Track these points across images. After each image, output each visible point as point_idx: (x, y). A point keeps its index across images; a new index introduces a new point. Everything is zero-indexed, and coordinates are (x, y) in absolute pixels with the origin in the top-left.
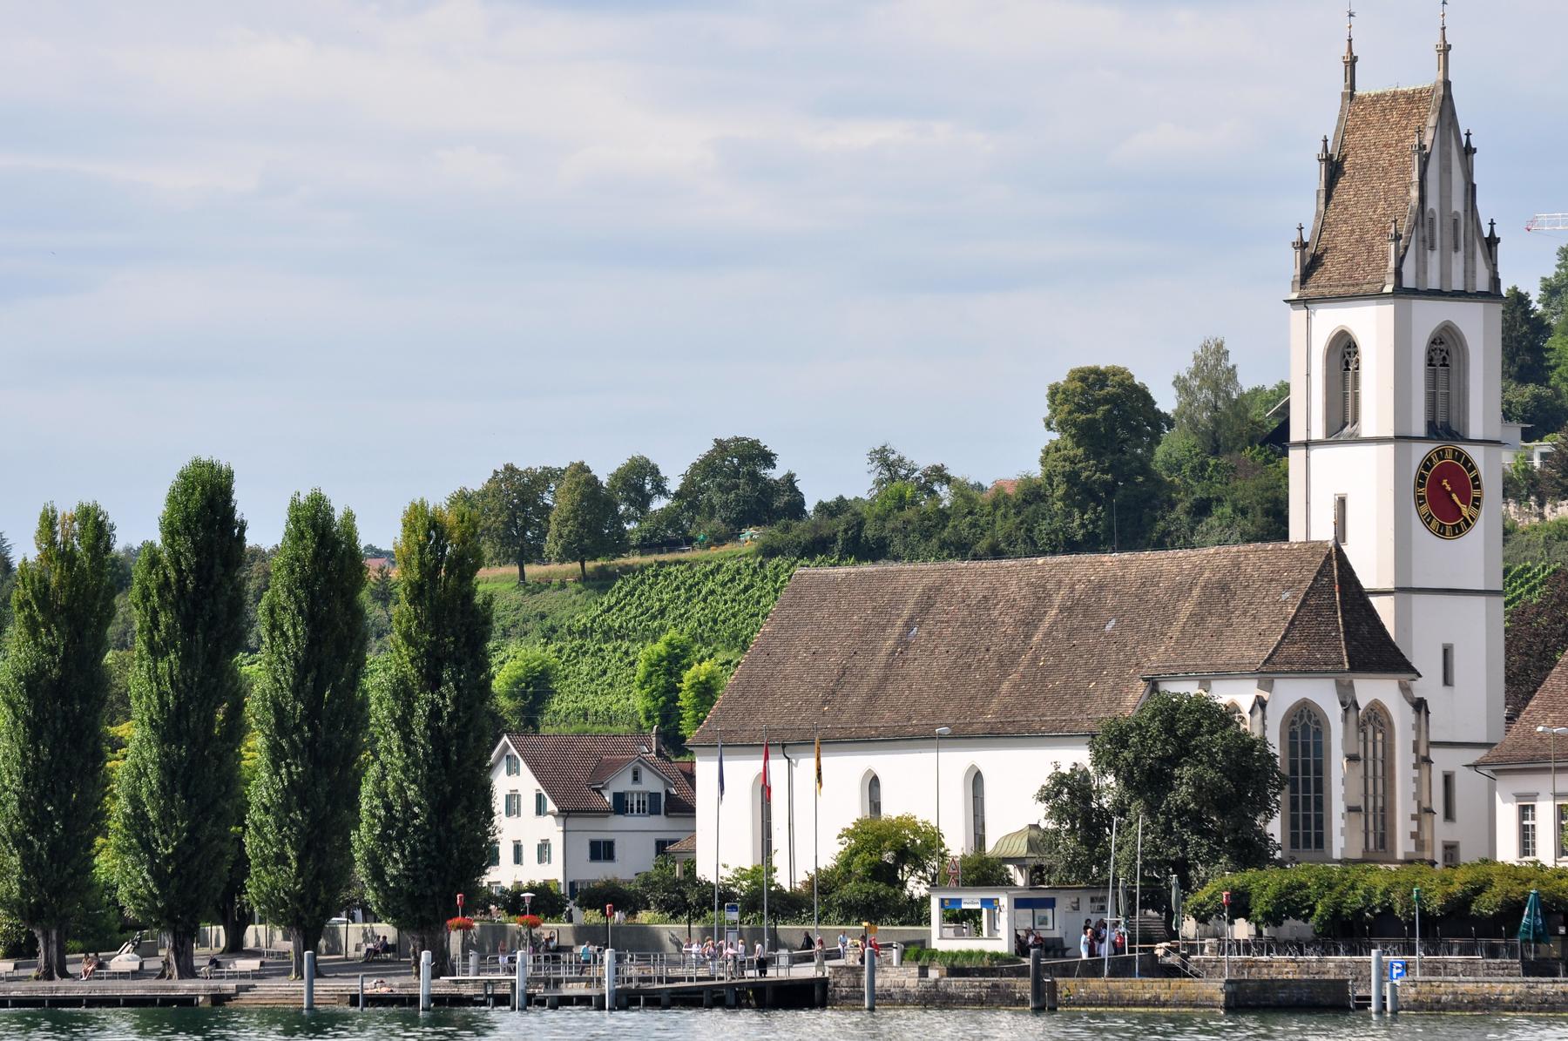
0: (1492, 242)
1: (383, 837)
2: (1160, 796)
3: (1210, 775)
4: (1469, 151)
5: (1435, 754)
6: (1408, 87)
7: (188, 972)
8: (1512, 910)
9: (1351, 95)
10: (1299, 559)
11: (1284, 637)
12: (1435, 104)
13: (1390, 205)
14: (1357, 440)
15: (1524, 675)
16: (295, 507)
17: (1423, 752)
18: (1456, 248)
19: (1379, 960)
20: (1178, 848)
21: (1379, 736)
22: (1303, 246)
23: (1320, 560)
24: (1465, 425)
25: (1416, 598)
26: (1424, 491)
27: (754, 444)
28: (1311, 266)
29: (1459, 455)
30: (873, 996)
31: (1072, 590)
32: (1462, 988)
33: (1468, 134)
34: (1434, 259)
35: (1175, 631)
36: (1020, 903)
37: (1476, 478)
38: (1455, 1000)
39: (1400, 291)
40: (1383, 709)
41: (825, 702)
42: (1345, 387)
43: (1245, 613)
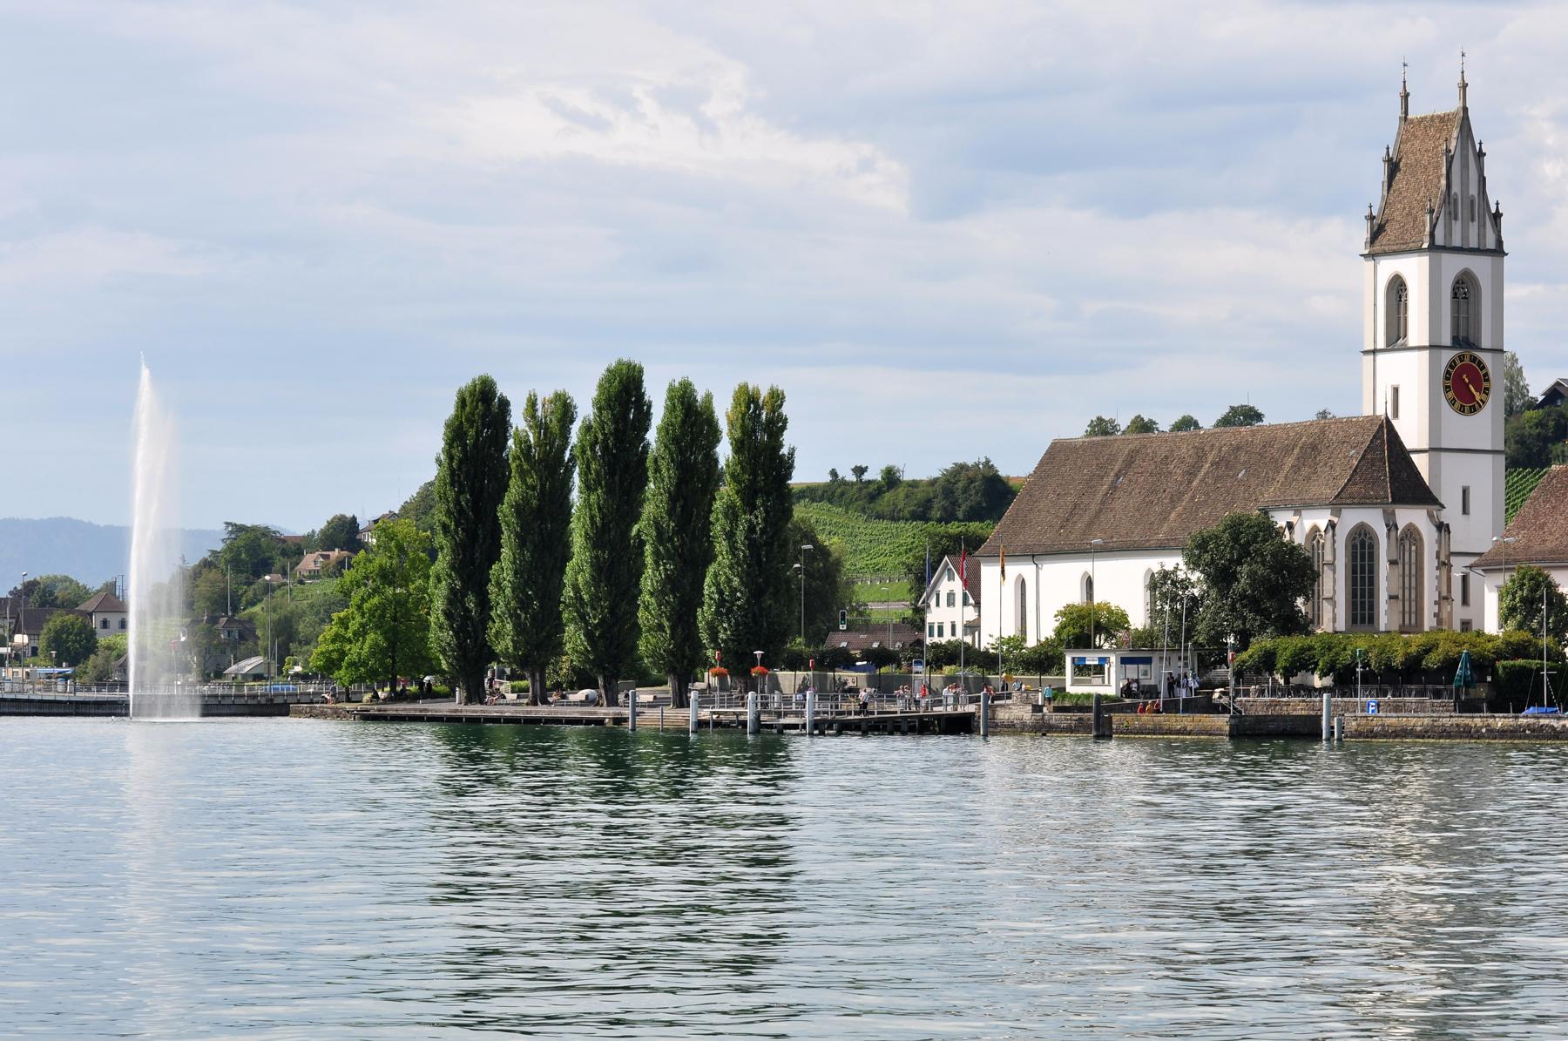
0: (1497, 216)
1: (717, 612)
2: (1229, 587)
4: (1481, 155)
5: (1453, 560)
6: (1441, 112)
7: (682, 702)
8: (1450, 665)
12: (1457, 123)
14: (1406, 348)
16: (671, 389)
19: (1329, 702)
22: (1371, 218)
24: (1479, 338)
25: (1443, 454)
26: (1449, 383)
27: (1252, 409)
28: (1377, 232)
29: (1474, 359)
30: (986, 727)
32: (1388, 721)
34: (1457, 227)
35: (1281, 477)
39: (1433, 247)
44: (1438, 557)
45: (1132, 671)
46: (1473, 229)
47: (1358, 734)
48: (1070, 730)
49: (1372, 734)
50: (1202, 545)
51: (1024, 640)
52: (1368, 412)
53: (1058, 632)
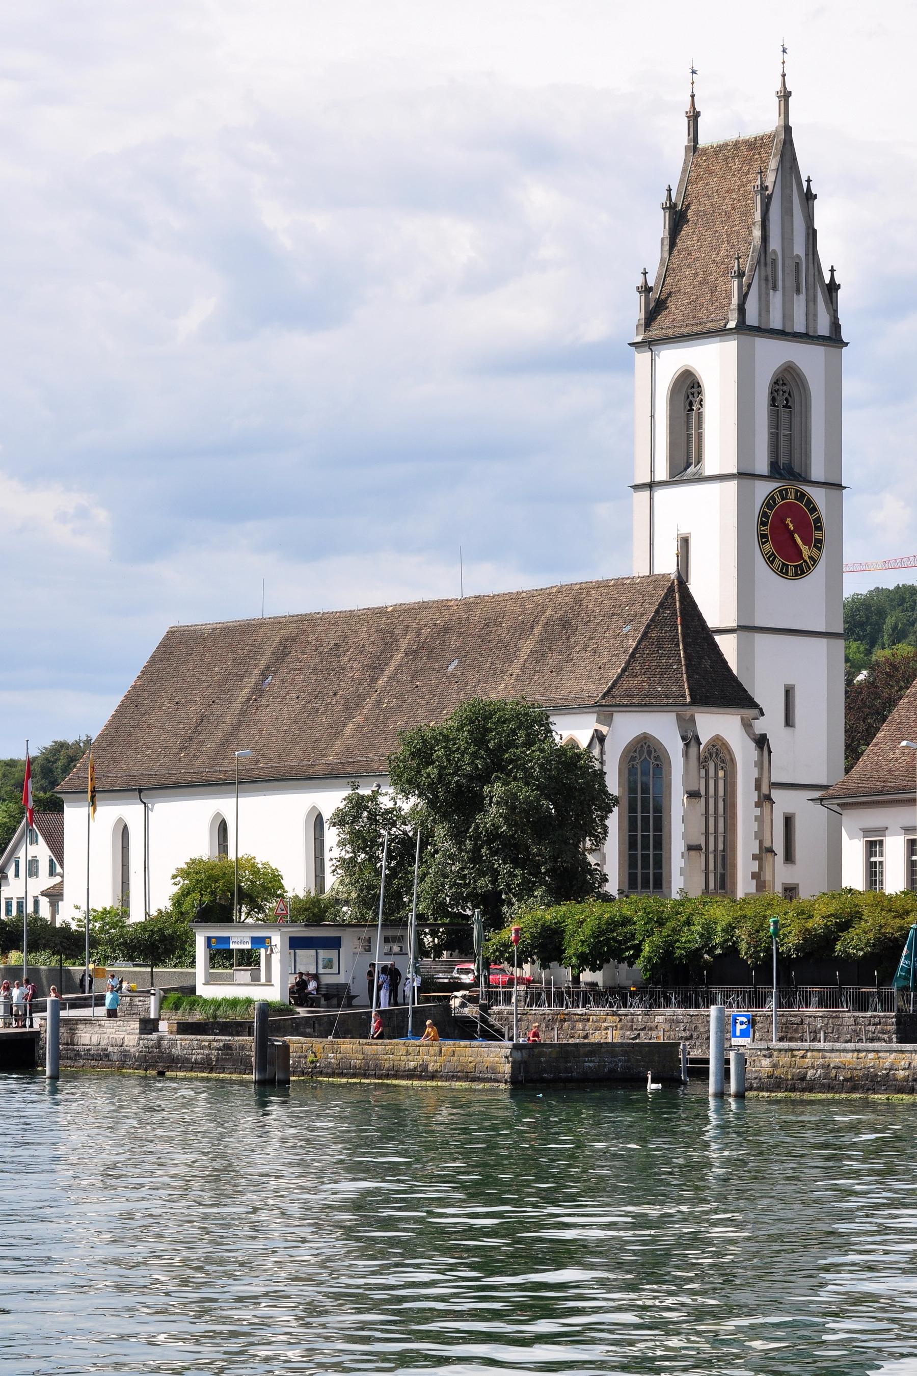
0: (833, 288)
2: (469, 818)
3: (525, 793)
5: (776, 794)
9: (693, 147)
10: (640, 592)
11: (624, 670)
13: (733, 246)
15: (864, 715)
17: (765, 789)
18: (798, 291)
20: (487, 878)
21: (721, 774)
22: (646, 290)
23: (662, 593)
24: (807, 466)
25: (759, 637)
26: (766, 530)
28: (655, 308)
29: (801, 496)
30: (57, 1057)
31: (419, 634)
32: (835, 1059)
33: (809, 181)
34: (776, 299)
37: (818, 520)
38: (826, 1076)
39: (743, 328)
40: (725, 745)
41: (181, 750)
42: (688, 428)
43: (585, 648)
44: (758, 787)
45: (307, 960)
46: (799, 304)
47: (775, 1083)
48: (207, 1065)
49: (802, 1083)
50: (423, 753)
51: (126, 914)
52: (640, 569)
53: (178, 901)
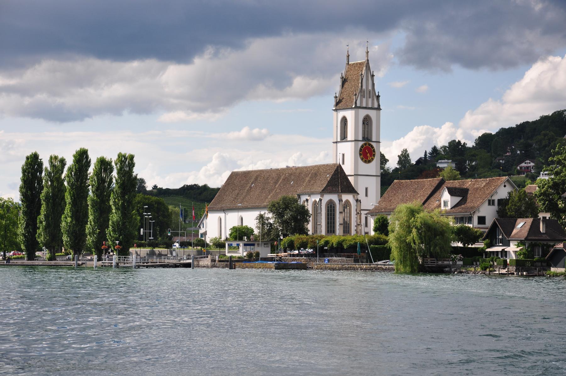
0: (378, 97)
17: (358, 211)
26: (361, 153)
29: (370, 145)
34: (364, 100)
36: (245, 245)
39: (356, 107)
40: (349, 201)
44: (356, 211)
46: (370, 101)
50: (274, 206)
